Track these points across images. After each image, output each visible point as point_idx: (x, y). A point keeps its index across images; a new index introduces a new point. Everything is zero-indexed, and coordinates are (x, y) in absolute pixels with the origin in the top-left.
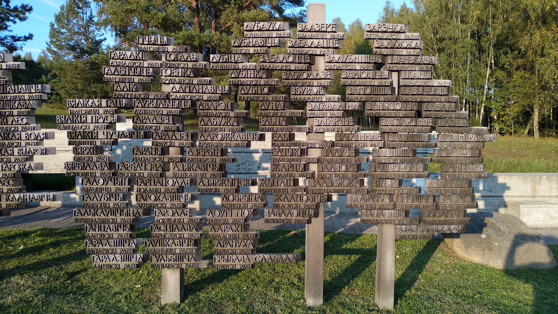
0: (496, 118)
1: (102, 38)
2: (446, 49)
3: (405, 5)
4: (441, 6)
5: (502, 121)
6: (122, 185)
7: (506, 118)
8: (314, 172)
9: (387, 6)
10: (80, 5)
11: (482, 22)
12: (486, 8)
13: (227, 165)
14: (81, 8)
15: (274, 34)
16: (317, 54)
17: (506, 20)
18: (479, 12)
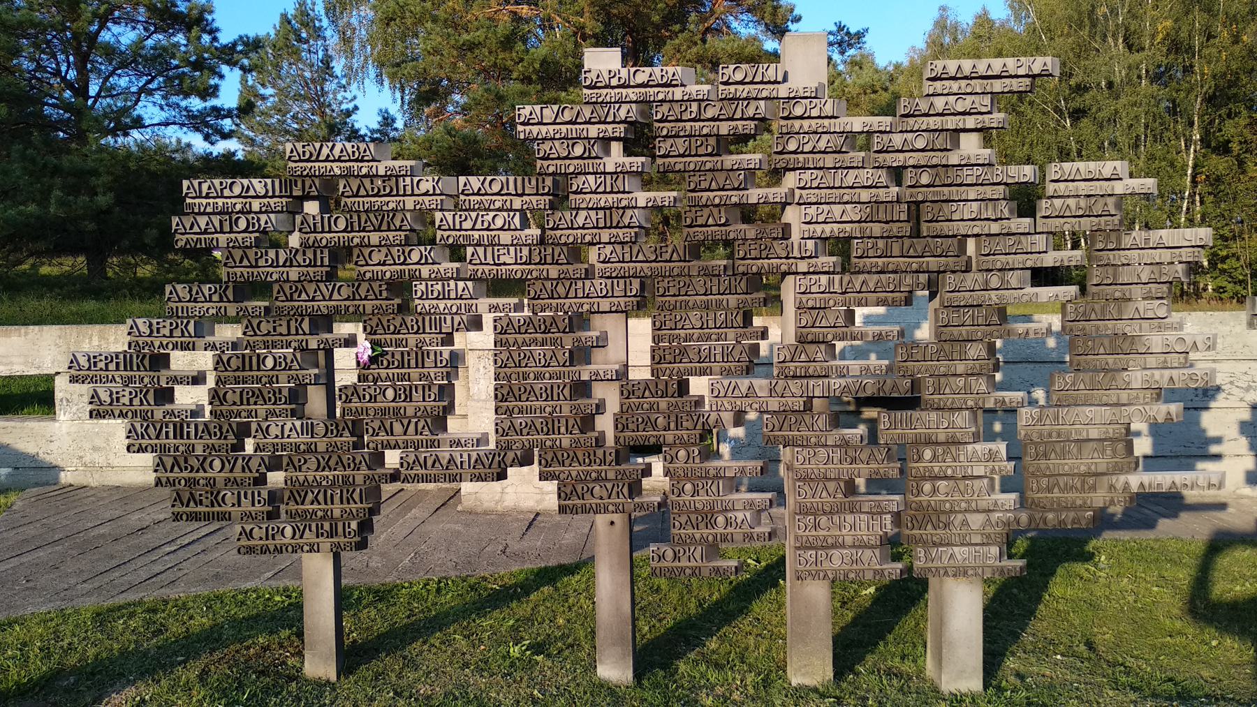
0: (1206, 264)
1: (351, 106)
2: (1094, 110)
3: (986, 13)
4: (1080, 13)
5: (1223, 271)
6: (182, 438)
7: (1231, 263)
8: (703, 397)
9: (942, 16)
10: (304, 35)
11: (1175, 46)
12: (1187, 13)
13: (178, 388)
14: (307, 42)
15: (632, 94)
16: (968, 127)
17: (1236, 40)
18: (1169, 23)
